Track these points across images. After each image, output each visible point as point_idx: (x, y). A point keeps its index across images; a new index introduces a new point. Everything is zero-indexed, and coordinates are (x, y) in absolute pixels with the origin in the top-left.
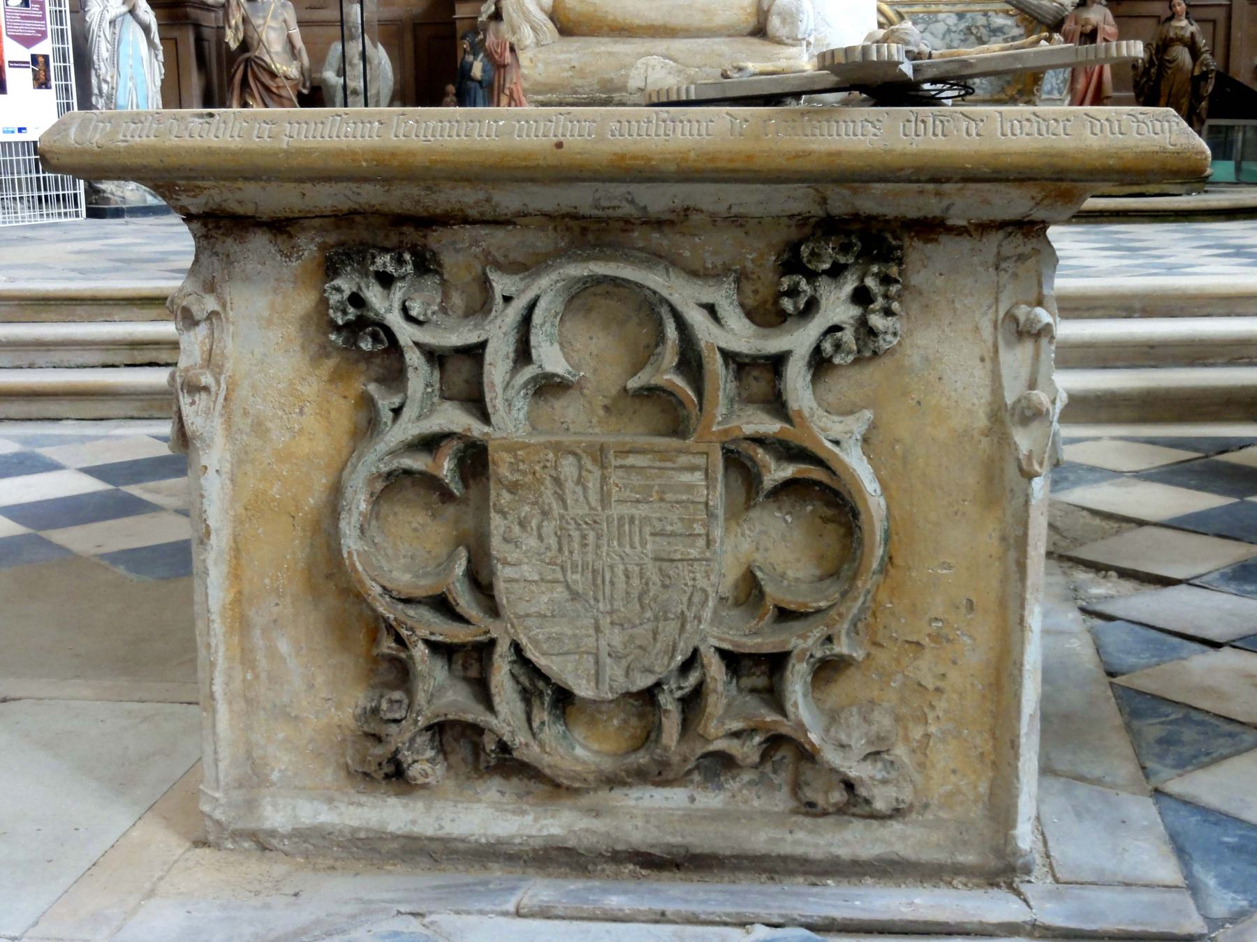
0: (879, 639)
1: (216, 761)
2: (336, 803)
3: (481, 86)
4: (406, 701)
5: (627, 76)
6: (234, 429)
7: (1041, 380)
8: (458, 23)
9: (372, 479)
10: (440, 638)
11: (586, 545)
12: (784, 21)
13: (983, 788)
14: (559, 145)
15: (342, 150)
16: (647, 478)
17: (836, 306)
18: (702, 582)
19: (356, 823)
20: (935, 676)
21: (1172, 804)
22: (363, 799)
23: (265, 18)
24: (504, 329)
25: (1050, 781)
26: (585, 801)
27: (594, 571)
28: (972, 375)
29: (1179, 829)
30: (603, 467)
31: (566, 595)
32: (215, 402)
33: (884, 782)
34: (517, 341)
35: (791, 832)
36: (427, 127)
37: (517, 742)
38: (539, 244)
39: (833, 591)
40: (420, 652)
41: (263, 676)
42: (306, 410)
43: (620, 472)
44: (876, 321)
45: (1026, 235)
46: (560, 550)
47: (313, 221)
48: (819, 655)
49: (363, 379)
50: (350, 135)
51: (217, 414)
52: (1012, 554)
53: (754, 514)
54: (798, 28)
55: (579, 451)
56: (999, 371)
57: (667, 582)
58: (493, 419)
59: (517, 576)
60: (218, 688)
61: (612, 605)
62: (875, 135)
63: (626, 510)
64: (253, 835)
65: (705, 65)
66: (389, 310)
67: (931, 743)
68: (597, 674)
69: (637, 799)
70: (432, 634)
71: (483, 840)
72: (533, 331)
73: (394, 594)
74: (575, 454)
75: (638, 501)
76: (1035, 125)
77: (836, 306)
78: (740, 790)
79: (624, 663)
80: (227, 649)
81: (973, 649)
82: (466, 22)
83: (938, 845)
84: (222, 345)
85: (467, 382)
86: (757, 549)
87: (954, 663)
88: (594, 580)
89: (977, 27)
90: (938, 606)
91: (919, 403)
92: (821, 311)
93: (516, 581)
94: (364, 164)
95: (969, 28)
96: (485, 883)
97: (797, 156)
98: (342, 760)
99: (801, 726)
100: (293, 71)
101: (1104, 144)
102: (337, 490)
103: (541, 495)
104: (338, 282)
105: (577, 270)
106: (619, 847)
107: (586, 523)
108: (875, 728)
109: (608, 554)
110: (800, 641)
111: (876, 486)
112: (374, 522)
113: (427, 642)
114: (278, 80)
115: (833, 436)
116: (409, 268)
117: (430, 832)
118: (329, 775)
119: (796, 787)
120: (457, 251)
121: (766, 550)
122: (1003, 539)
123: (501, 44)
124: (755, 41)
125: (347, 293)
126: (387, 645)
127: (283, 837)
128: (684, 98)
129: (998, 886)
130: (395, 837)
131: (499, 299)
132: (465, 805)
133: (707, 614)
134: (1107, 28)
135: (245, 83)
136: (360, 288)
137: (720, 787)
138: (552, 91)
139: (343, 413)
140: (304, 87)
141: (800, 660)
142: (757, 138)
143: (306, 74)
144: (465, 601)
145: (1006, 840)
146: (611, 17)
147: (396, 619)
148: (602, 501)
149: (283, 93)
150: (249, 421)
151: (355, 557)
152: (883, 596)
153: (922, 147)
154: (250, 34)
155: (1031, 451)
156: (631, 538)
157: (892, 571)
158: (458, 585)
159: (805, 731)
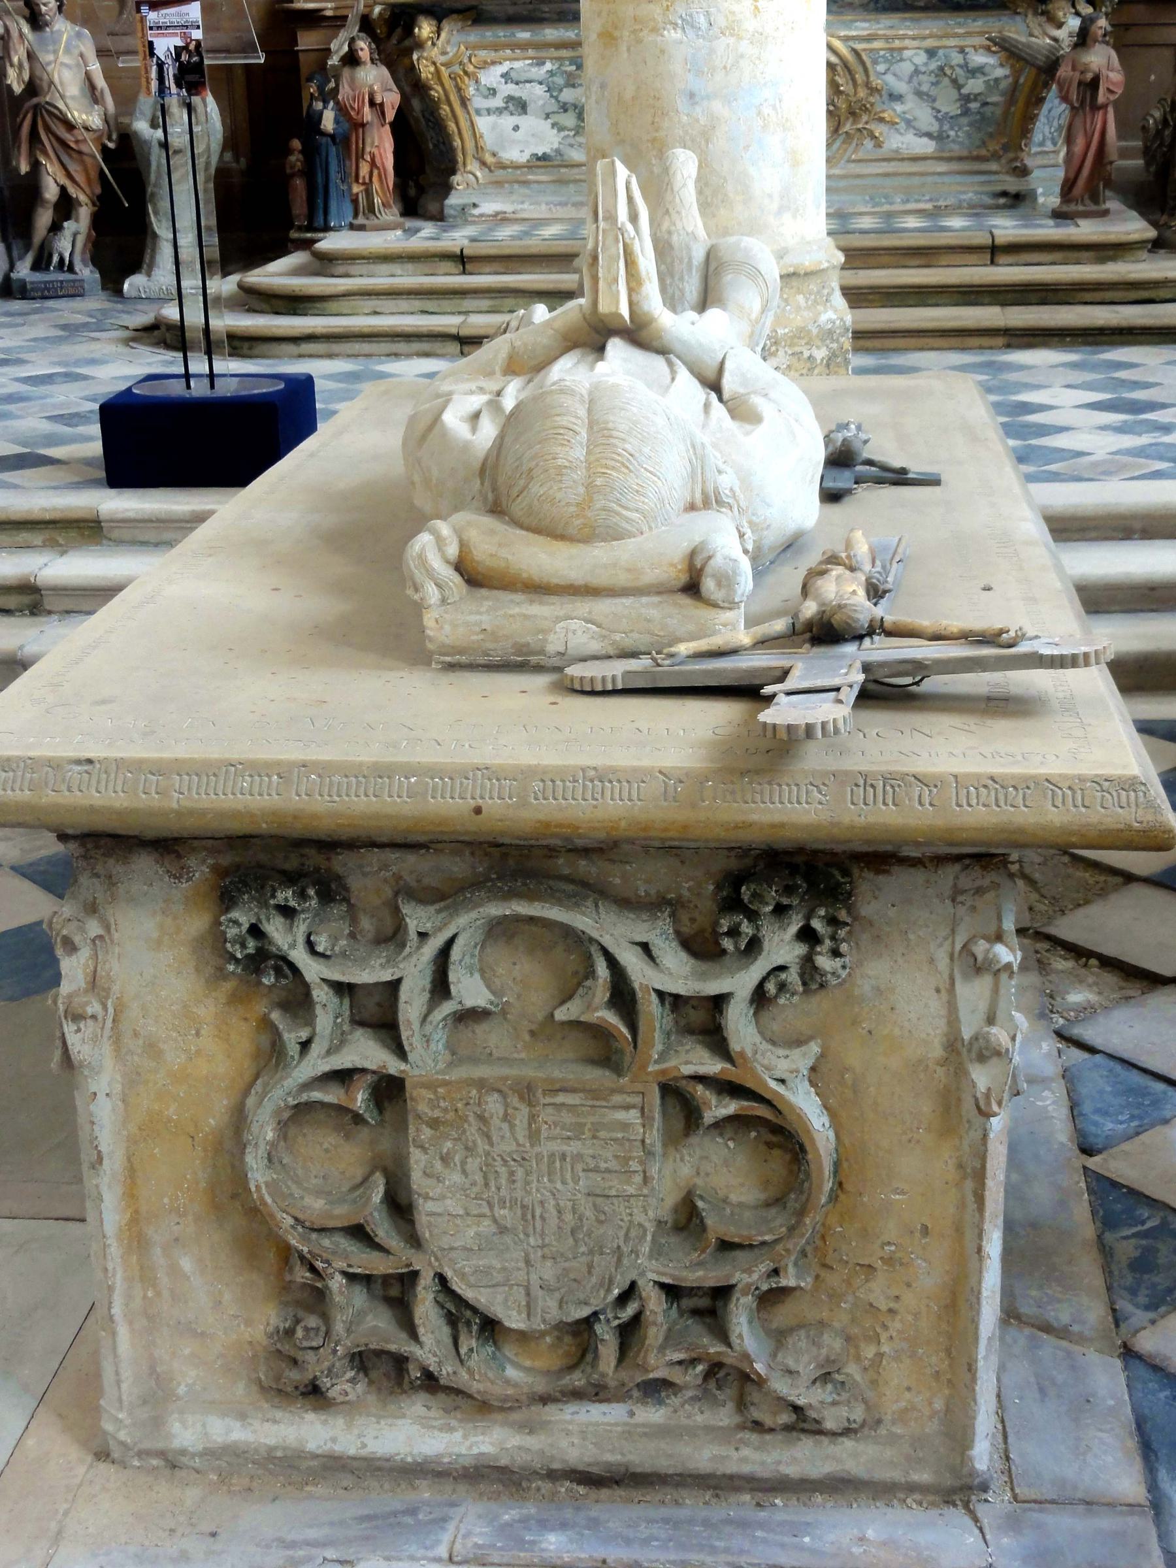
0: (828, 1261)
1: (118, 1383)
2: (249, 1420)
3: (334, 143)
4: (323, 1329)
5: (545, 640)
6: (124, 1051)
7: (1000, 1015)
8: (301, 56)
9: (278, 1112)
10: (359, 1271)
11: (514, 1181)
12: (719, 584)
13: (939, 1405)
14: (478, 811)
15: (239, 811)
16: (578, 1116)
17: (781, 947)
18: (639, 1218)
19: (271, 1441)
20: (888, 1298)
21: (1142, 1371)
22: (279, 1414)
23: (56, 52)
24: (419, 968)
25: (1013, 1332)
26: (516, 1416)
27: (523, 1207)
28: (926, 1006)
29: (1146, 1411)
30: (530, 1105)
31: (494, 1229)
32: (103, 1028)
33: (834, 1403)
34: (434, 972)
35: (737, 1449)
36: (331, 784)
37: (444, 1372)
38: (456, 869)
39: (779, 1222)
40: (337, 1283)
41: (166, 1294)
42: (203, 1032)
43: (550, 1110)
44: (824, 962)
45: (984, 868)
46: (487, 1185)
47: (204, 842)
48: (765, 1287)
49: (265, 1001)
50: (246, 791)
51: (105, 1039)
52: (969, 1185)
53: (694, 1140)
54: (735, 591)
55: (504, 1089)
56: (956, 1003)
57: (603, 1218)
58: (411, 1057)
59: (439, 1210)
60: (117, 1310)
61: (543, 1239)
62: (820, 803)
63: (556, 1147)
64: (161, 1454)
65: (632, 631)
66: (293, 946)
67: (884, 1362)
68: (528, 1305)
69: (573, 1414)
70: (350, 1266)
71: (409, 1459)
72: (451, 967)
73: (307, 1224)
74: (499, 1091)
75: (569, 1138)
76: (993, 793)
77: (781, 947)
78: (682, 1406)
79: (557, 1295)
80: (125, 1271)
81: (929, 1274)
82: (313, 55)
83: (892, 1462)
84: (107, 966)
85: (379, 1005)
86: (698, 1174)
87: (909, 1285)
88: (524, 1216)
89: (952, 67)
90: (891, 1230)
91: (870, 1032)
92: (764, 953)
93: (439, 1215)
94: (264, 826)
95: (941, 69)
96: (412, 1511)
97: (736, 827)
98: (254, 1376)
99: (746, 1357)
100: (95, 120)
101: (1066, 819)
102: (239, 1119)
103: (464, 1131)
104: (235, 914)
105: (495, 910)
106: (556, 1466)
107: (514, 1160)
108: (824, 1351)
109: (538, 1190)
110: (745, 1276)
111: (825, 1119)
112: (282, 1143)
113: (345, 1274)
114: (76, 132)
115: (778, 1075)
116: (314, 903)
117: (352, 1452)
118: (240, 1389)
119: (742, 1404)
120: (365, 875)
121: (707, 1174)
122: (960, 1166)
123: (358, 98)
124: (685, 600)
125: (246, 926)
126: (302, 1275)
127: (193, 1455)
128: (610, 687)
129: (955, 1505)
130: (316, 1456)
131: (412, 935)
132: (390, 1421)
133: (646, 1248)
134: (1112, 75)
135: (34, 136)
136: (259, 920)
137: (661, 1402)
138: (460, 653)
139: (244, 1036)
140: (110, 139)
141: (745, 1294)
142: (694, 806)
143: (112, 123)
144: (383, 1229)
145: (962, 1462)
146: (525, 575)
147: (309, 1252)
148: (530, 1137)
149: (84, 148)
150: (141, 1042)
151: (264, 1191)
152: (833, 1220)
153: (871, 819)
154: (38, 73)
155: (989, 1089)
156: (562, 1175)
157: (842, 1197)
158: (376, 1214)
159: (751, 1363)
